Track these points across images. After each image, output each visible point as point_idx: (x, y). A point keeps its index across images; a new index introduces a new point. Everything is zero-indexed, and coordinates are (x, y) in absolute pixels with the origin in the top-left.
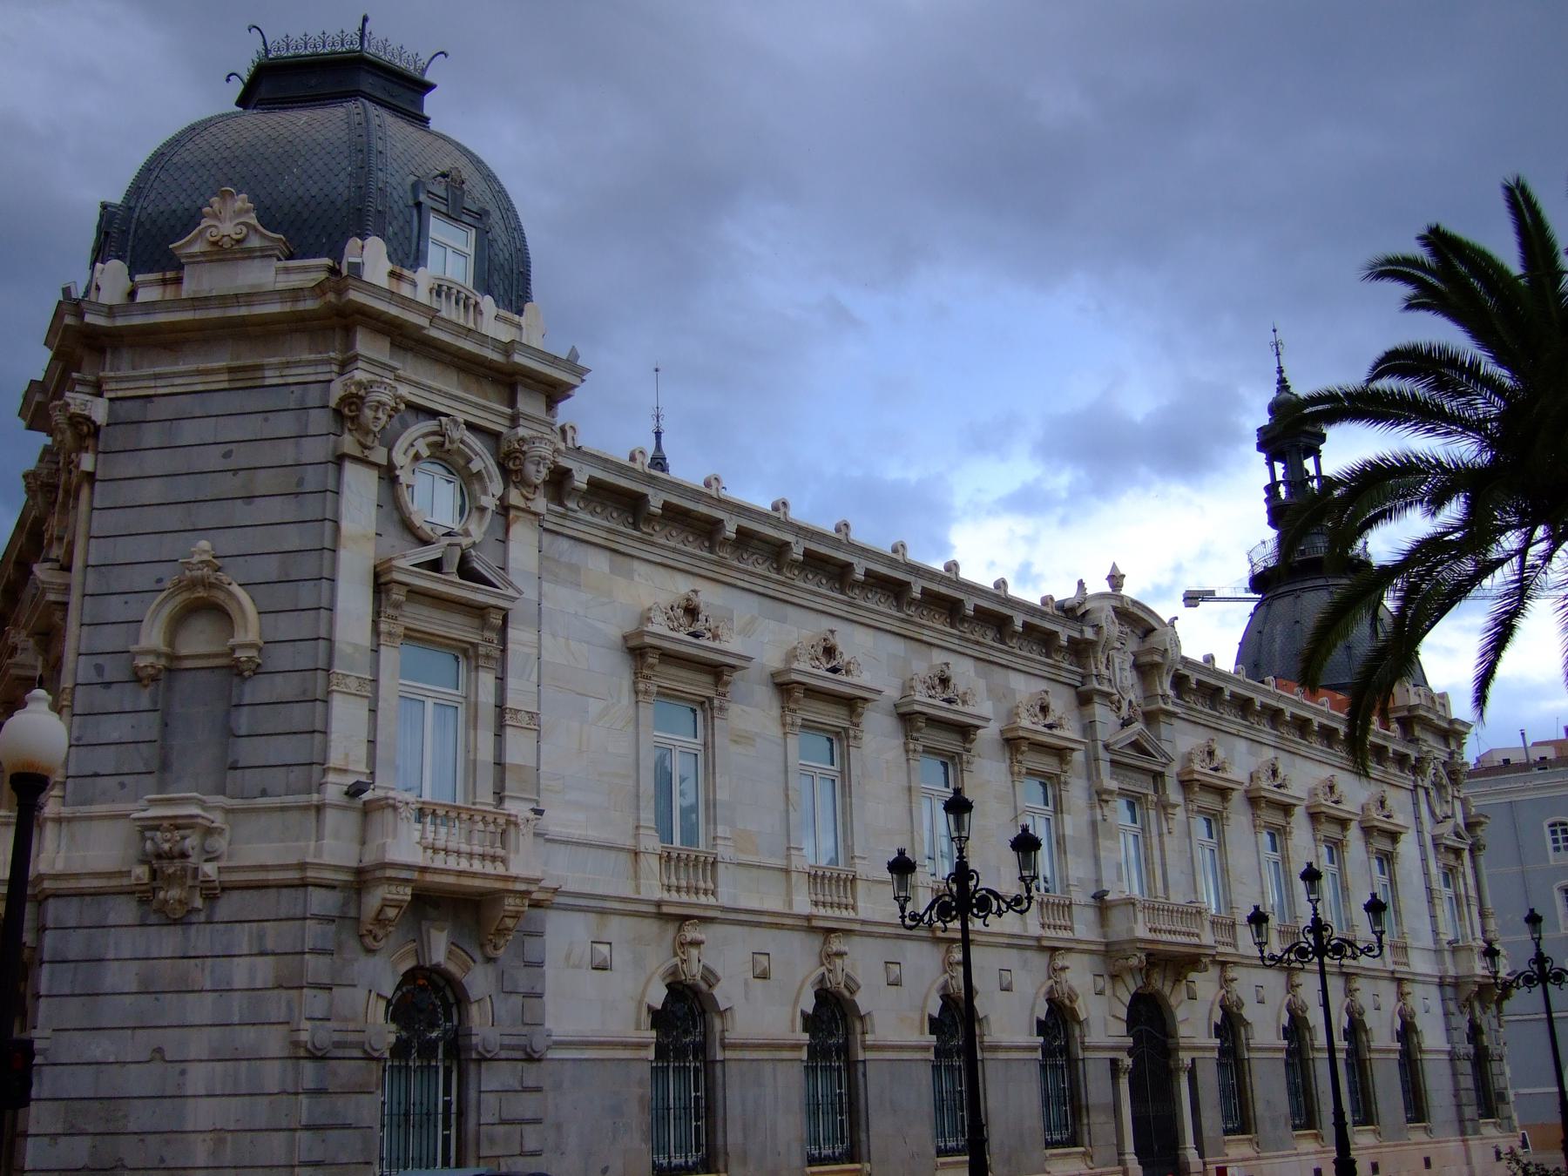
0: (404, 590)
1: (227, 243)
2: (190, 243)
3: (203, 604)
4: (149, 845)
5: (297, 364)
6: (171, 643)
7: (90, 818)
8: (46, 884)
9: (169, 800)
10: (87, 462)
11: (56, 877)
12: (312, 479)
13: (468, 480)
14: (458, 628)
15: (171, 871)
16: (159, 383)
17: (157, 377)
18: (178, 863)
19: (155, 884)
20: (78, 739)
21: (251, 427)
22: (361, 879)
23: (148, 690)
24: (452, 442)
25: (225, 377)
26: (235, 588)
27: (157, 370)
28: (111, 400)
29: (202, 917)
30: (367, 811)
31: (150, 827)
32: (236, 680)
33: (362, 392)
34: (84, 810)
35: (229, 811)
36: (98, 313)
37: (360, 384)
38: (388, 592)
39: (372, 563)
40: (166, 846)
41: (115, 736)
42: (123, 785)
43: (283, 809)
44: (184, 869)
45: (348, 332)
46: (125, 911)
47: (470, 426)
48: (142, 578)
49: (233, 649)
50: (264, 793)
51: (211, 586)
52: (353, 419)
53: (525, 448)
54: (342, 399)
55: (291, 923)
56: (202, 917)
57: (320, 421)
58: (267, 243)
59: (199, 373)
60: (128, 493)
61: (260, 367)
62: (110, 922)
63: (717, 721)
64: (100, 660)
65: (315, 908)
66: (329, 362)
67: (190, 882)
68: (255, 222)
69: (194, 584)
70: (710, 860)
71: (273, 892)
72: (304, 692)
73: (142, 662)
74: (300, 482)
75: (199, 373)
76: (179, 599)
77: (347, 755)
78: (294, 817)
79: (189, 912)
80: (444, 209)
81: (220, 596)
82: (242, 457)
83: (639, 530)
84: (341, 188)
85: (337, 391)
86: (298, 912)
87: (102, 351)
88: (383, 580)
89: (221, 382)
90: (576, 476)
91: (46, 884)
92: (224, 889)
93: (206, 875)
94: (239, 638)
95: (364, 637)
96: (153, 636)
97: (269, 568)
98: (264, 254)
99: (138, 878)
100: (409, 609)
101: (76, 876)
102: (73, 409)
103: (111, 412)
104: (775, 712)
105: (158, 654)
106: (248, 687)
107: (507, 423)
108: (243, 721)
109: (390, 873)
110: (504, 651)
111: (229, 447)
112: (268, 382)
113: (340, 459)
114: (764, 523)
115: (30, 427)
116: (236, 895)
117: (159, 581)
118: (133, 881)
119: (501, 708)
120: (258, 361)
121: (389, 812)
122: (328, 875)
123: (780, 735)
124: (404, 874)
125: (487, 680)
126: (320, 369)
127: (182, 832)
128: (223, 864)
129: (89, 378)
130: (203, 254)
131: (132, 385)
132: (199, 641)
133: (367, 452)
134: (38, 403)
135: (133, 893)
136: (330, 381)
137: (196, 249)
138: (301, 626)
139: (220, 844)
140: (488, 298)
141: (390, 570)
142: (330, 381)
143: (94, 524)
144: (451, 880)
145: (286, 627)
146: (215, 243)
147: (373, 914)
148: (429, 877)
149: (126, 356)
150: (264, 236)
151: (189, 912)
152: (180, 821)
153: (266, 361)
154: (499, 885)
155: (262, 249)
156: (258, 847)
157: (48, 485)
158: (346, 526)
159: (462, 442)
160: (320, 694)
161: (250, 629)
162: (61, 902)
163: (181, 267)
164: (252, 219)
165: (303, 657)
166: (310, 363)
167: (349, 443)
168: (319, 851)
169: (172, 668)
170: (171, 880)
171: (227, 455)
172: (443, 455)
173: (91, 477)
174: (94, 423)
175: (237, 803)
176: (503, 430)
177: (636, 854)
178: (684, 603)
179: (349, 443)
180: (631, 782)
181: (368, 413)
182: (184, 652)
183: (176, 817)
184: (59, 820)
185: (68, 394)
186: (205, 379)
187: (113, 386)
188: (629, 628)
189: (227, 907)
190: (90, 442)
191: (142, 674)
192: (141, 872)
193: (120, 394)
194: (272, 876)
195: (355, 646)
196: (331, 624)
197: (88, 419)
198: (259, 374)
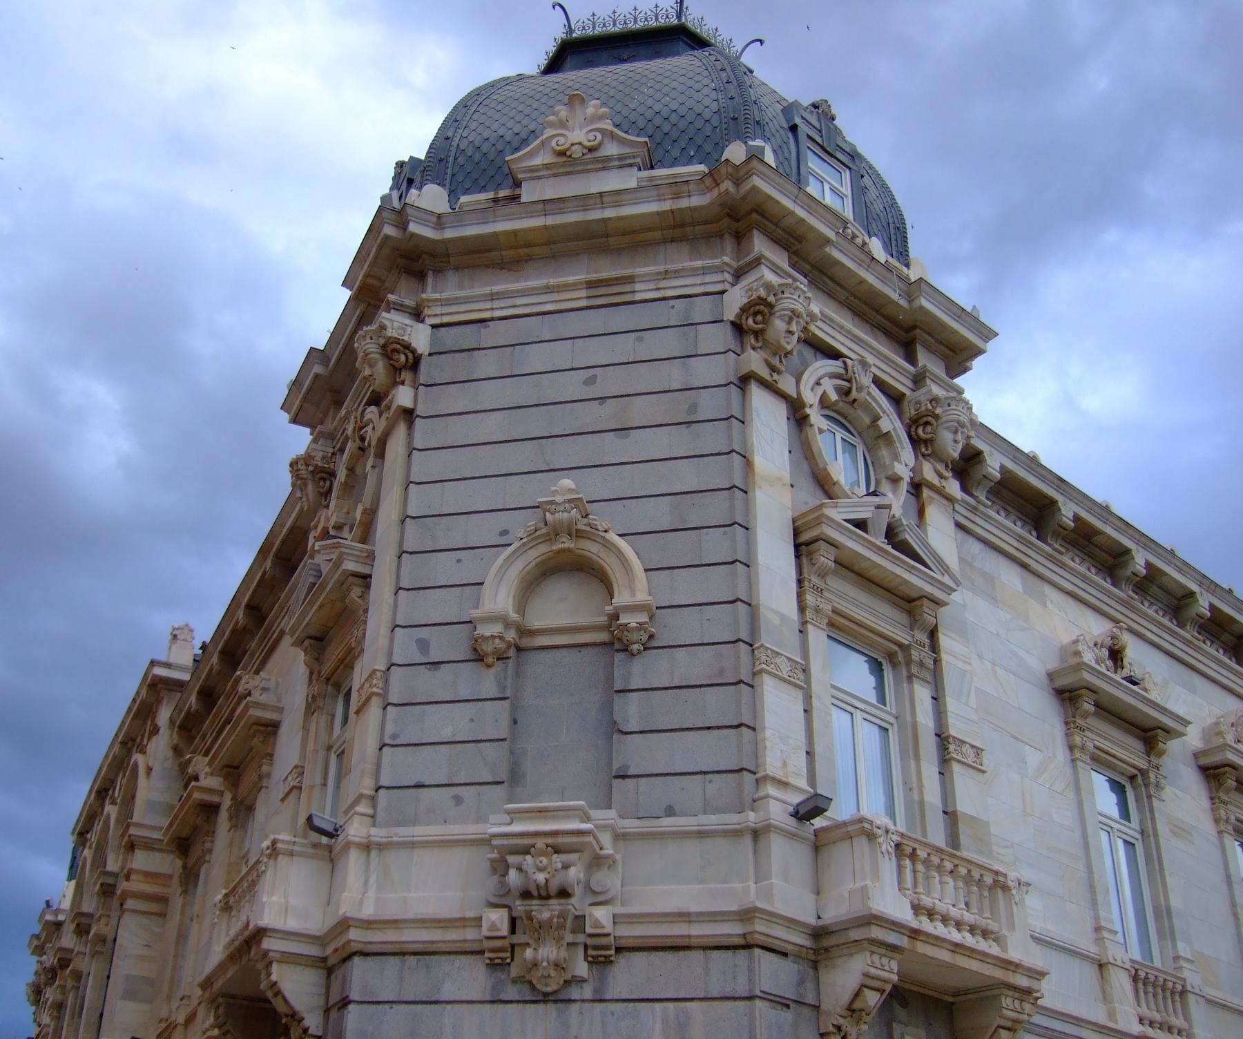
0: (832, 553)
1: (577, 152)
2: (531, 154)
3: (568, 560)
4: (513, 875)
5: (678, 273)
6: (521, 608)
7: (412, 845)
8: (354, 934)
9: (540, 811)
10: (403, 396)
11: (368, 924)
12: (709, 405)
13: (875, 439)
14: (885, 620)
15: (546, 915)
16: (496, 304)
17: (493, 297)
18: (555, 905)
19: (515, 939)
20: (394, 737)
21: (623, 348)
22: (822, 945)
23: (493, 670)
24: (860, 389)
25: (584, 293)
26: (612, 536)
27: (495, 288)
28: (433, 327)
29: (587, 992)
30: (819, 844)
31: (506, 852)
32: (619, 657)
33: (771, 299)
34: (404, 833)
35: (620, 837)
36: (424, 223)
37: (769, 287)
38: (810, 555)
39: (789, 515)
40: (541, 877)
41: (446, 734)
42: (458, 800)
43: (702, 835)
44: (563, 915)
45: (740, 237)
46: (468, 978)
47: (878, 382)
48: (483, 530)
49: (616, 616)
50: (670, 812)
51: (580, 535)
52: (757, 334)
53: (938, 411)
54: (744, 310)
55: (730, 1004)
56: (587, 992)
57: (720, 337)
58: (626, 150)
59: (549, 289)
60: (459, 430)
61: (630, 280)
62: (446, 994)
63: (1155, 803)
64: (424, 633)
65: (766, 983)
66: (719, 270)
67: (569, 938)
68: (610, 127)
69: (555, 532)
70: (1179, 988)
71: (697, 956)
72: (721, 671)
73: (485, 630)
74: (693, 408)
75: (549, 289)
76: (543, 549)
77: (785, 764)
78: (719, 846)
79: (567, 983)
80: (819, 140)
81: (591, 549)
82: (611, 382)
83: (1046, 543)
84: (707, 102)
85: (735, 299)
86: (742, 989)
87: (420, 276)
88: (804, 538)
89: (580, 297)
90: (989, 461)
91: (354, 934)
92: (619, 950)
93: (597, 924)
94: (622, 598)
95: (790, 608)
96: (499, 598)
97: (660, 514)
98: (623, 163)
99: (493, 927)
100: (835, 583)
101: (395, 923)
102: (391, 333)
103: (434, 340)
104: (1205, 803)
105: (508, 625)
106: (637, 666)
107: (910, 384)
108: (631, 712)
109: (876, 933)
110: (936, 661)
111: (592, 372)
112: (638, 297)
113: (744, 381)
114: (1169, 563)
115: (295, 420)
116: (639, 959)
117: (504, 533)
118: (485, 932)
119: (943, 739)
120: (628, 272)
121: (861, 844)
122: (780, 932)
123: (1215, 833)
124: (892, 938)
125: (923, 694)
126: (708, 278)
127: (564, 857)
128: (619, 910)
129: (407, 302)
130: (546, 166)
131: (463, 308)
132: (563, 608)
133: (775, 376)
134: (317, 376)
135: (481, 952)
136: (723, 292)
137: (538, 161)
138: (714, 585)
139: (609, 880)
140: (874, 239)
141: (818, 521)
142: (723, 292)
143: (415, 468)
144: (944, 955)
145: (687, 587)
146: (562, 153)
147: (846, 998)
148: (921, 948)
149: (452, 278)
150: (622, 142)
151: (567, 983)
152: (560, 840)
153: (638, 271)
154: (999, 974)
155: (620, 158)
156: (662, 886)
157: (323, 470)
158: (759, 461)
159: (869, 394)
160: (745, 675)
161: (635, 589)
162: (370, 963)
163: (518, 184)
164: (607, 125)
165: (720, 624)
166: (695, 272)
167: (755, 361)
168: (768, 895)
169: (518, 648)
170: (541, 930)
171: (591, 381)
172: (845, 409)
173: (409, 415)
174: (413, 351)
175: (630, 825)
176: (907, 392)
177: (1101, 966)
178: (1108, 642)
179: (755, 361)
180: (1081, 866)
181: (779, 325)
182: (538, 624)
183: (555, 833)
184: (367, 847)
185: (384, 314)
186: (555, 297)
187: (438, 310)
188: (1053, 664)
189: (628, 975)
190: (406, 375)
191: (487, 648)
192: (497, 919)
193: (446, 319)
194: (697, 930)
195: (783, 617)
196: (751, 584)
197: (407, 347)
198: (627, 288)
